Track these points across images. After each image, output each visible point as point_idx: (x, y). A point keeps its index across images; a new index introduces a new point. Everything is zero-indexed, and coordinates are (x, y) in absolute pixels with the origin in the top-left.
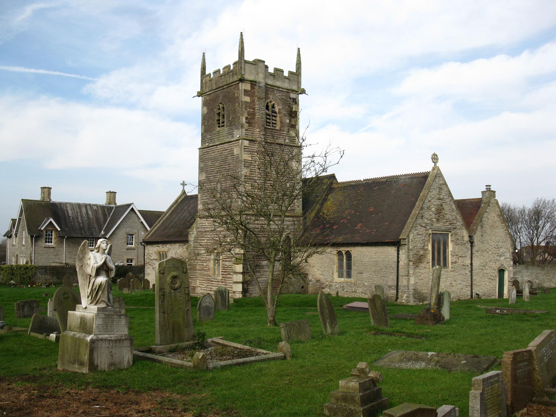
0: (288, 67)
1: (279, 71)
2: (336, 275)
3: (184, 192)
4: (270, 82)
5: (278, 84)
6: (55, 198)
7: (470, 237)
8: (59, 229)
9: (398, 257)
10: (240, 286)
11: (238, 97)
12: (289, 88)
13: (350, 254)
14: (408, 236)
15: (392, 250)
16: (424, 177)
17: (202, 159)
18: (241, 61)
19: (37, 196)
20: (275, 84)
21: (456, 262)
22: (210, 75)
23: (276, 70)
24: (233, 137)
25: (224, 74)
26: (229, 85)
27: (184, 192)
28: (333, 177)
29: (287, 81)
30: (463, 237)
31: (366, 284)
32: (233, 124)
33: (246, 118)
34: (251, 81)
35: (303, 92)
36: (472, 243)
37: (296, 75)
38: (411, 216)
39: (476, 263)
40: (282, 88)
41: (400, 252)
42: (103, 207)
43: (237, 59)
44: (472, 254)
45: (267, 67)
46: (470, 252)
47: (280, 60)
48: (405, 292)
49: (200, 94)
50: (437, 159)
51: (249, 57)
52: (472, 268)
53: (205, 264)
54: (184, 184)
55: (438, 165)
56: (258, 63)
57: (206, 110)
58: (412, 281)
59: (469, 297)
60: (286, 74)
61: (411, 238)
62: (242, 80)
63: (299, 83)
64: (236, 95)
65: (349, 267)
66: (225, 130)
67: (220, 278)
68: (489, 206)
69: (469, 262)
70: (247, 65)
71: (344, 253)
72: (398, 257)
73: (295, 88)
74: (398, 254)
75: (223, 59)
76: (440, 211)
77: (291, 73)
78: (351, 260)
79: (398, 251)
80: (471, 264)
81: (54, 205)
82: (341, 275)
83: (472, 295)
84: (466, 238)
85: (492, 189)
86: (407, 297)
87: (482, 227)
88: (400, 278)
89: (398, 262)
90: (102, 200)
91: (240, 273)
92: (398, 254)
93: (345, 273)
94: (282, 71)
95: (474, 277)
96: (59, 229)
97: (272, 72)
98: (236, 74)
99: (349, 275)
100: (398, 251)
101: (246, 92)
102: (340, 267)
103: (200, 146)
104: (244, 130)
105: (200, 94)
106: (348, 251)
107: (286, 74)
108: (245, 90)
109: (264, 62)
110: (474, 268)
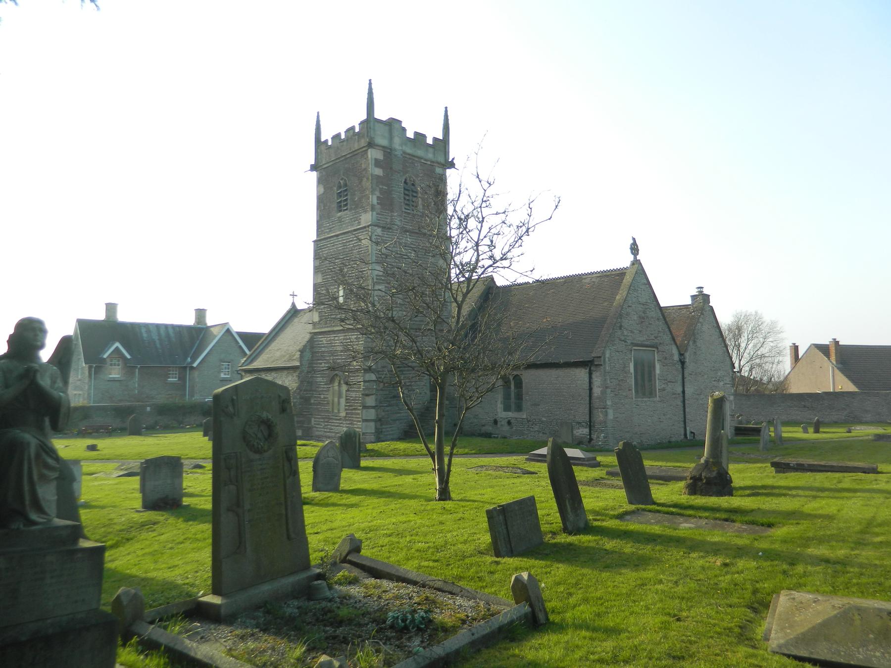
0: (433, 132)
1: (420, 137)
2: (500, 406)
3: (293, 305)
4: (409, 151)
5: (420, 153)
6: (123, 316)
7: (681, 355)
8: (129, 357)
9: (590, 383)
10: (372, 424)
11: (365, 169)
12: (434, 160)
13: (521, 380)
14: (604, 353)
15: (582, 374)
16: (620, 274)
17: (317, 256)
18: (370, 121)
19: (99, 315)
20: (415, 154)
21: (664, 390)
22: (326, 141)
23: (416, 133)
24: (359, 223)
25: (348, 139)
26: (354, 154)
27: (293, 305)
28: (205, 435)
29: (431, 150)
30: (672, 355)
31: (544, 419)
32: (358, 207)
33: (378, 197)
34: (383, 147)
35: (452, 165)
36: (683, 363)
37: (443, 144)
38: (606, 326)
39: (689, 390)
40: (426, 160)
41: (593, 376)
42: (189, 328)
43: (364, 117)
44: (683, 378)
45: (404, 130)
46: (680, 376)
47: (422, 123)
48: (602, 431)
49: (313, 168)
50: (638, 250)
51: (381, 114)
52: (684, 397)
53: (322, 396)
54: (293, 295)
55: (638, 257)
56: (393, 125)
57: (322, 190)
58: (611, 416)
59: (683, 437)
60: (430, 141)
61: (607, 355)
62: (371, 145)
63: (446, 152)
64: (363, 166)
65: (519, 397)
66: (346, 215)
67: (343, 414)
68: (702, 314)
69: (680, 389)
70: (377, 125)
71: (511, 378)
72: (590, 383)
73: (441, 159)
74: (590, 378)
75: (342, 119)
76: (642, 320)
77: (435, 139)
78: (521, 387)
79: (590, 374)
80: (684, 392)
81: (123, 325)
82: (507, 408)
83: (685, 435)
84: (676, 357)
85: (706, 292)
86: (605, 437)
87: (695, 342)
88: (595, 412)
89: (591, 389)
90: (189, 320)
91: (373, 407)
92: (590, 378)
93: (513, 406)
94: (424, 136)
95: (687, 410)
96: (129, 357)
97: (412, 137)
98: (363, 137)
99: (519, 408)
100: (590, 374)
101: (377, 163)
102: (507, 397)
103: (315, 238)
104: (374, 213)
105: (313, 168)
106: (517, 375)
107: (430, 141)
108: (376, 160)
109: (400, 122)
110: (686, 397)
